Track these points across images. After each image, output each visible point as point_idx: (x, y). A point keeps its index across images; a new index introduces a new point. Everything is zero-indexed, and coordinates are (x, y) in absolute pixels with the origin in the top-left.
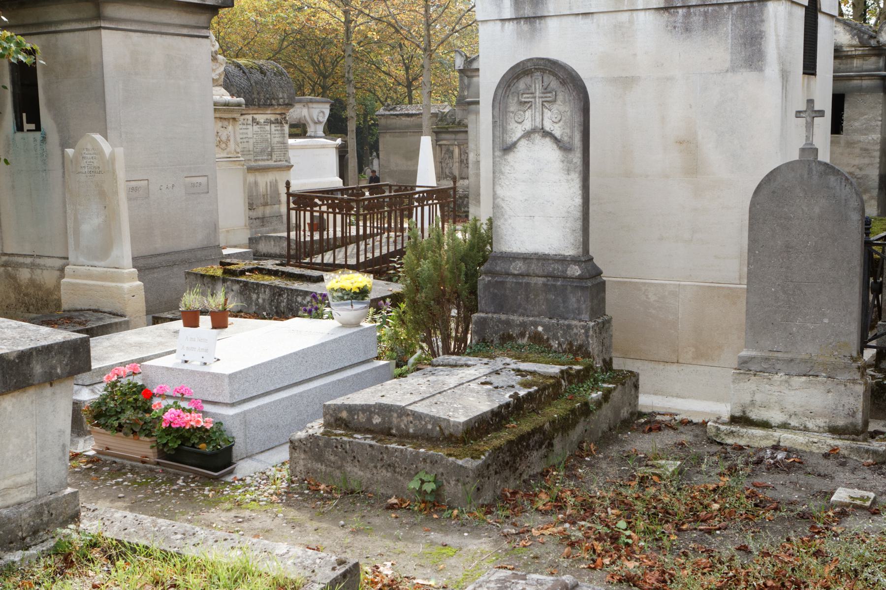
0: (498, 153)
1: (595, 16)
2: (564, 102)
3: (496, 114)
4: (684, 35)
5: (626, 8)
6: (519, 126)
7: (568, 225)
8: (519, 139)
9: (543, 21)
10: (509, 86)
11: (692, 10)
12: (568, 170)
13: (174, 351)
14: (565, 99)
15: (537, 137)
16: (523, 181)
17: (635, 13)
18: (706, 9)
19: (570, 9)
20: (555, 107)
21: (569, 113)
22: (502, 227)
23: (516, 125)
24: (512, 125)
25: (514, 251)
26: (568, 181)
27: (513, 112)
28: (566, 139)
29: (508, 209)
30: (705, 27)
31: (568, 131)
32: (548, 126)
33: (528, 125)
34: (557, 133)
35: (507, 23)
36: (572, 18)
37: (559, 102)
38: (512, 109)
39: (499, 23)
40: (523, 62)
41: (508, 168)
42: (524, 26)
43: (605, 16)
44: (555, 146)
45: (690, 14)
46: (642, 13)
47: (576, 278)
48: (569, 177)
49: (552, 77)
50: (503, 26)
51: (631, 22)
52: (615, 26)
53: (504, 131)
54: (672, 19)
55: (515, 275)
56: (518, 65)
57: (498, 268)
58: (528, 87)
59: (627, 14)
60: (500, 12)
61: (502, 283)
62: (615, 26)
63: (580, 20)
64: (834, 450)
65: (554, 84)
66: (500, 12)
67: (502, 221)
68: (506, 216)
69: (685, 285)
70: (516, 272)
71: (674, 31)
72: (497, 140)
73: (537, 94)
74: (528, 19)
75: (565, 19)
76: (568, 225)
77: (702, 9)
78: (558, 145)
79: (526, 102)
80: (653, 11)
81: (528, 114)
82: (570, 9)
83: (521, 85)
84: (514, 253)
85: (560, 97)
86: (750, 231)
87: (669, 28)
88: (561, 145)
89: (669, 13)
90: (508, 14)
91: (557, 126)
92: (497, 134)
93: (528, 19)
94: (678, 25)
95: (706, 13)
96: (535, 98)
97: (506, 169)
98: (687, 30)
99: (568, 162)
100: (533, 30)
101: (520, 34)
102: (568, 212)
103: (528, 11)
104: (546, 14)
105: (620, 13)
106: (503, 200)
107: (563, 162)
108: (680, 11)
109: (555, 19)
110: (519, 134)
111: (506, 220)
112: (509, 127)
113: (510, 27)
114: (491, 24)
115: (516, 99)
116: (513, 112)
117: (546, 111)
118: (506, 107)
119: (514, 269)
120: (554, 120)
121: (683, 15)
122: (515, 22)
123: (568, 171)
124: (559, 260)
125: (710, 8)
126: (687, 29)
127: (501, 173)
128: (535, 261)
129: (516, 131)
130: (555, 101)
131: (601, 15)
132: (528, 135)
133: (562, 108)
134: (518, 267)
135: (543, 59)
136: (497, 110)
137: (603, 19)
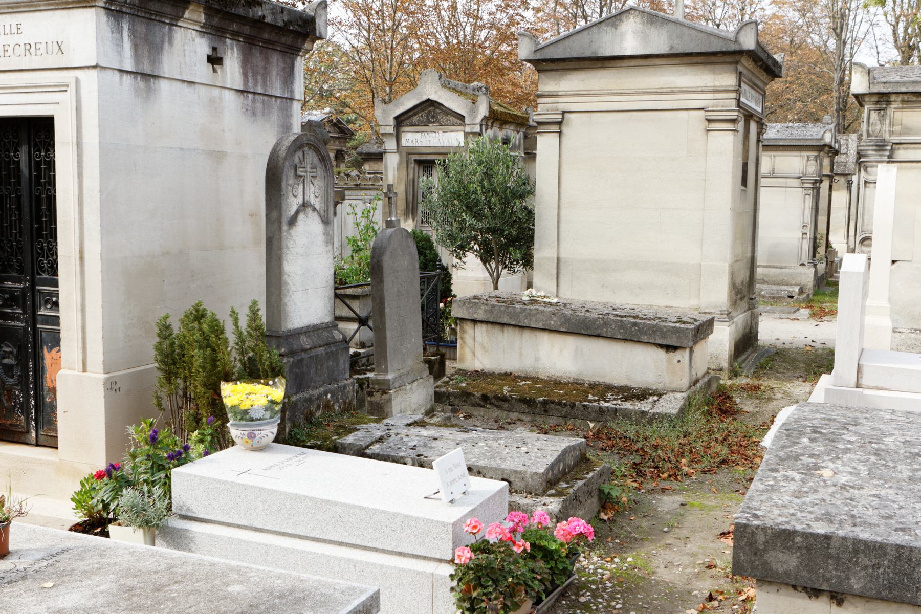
1: (197, 86)
8: (297, 213)
9: (156, 82)
11: (257, 97)
13: (84, 371)
17: (224, 91)
36: (179, 84)
39: (117, 74)
42: (141, 84)
59: (218, 90)
61: (301, 360)
63: (185, 88)
64: (621, 584)
66: (121, 62)
80: (234, 92)
84: (298, 329)
86: (297, 498)
90: (129, 66)
91: (317, 200)
103: (147, 69)
105: (213, 88)
109: (166, 81)
113: (127, 79)
114: (110, 72)
129: (292, 203)
137: (202, 90)
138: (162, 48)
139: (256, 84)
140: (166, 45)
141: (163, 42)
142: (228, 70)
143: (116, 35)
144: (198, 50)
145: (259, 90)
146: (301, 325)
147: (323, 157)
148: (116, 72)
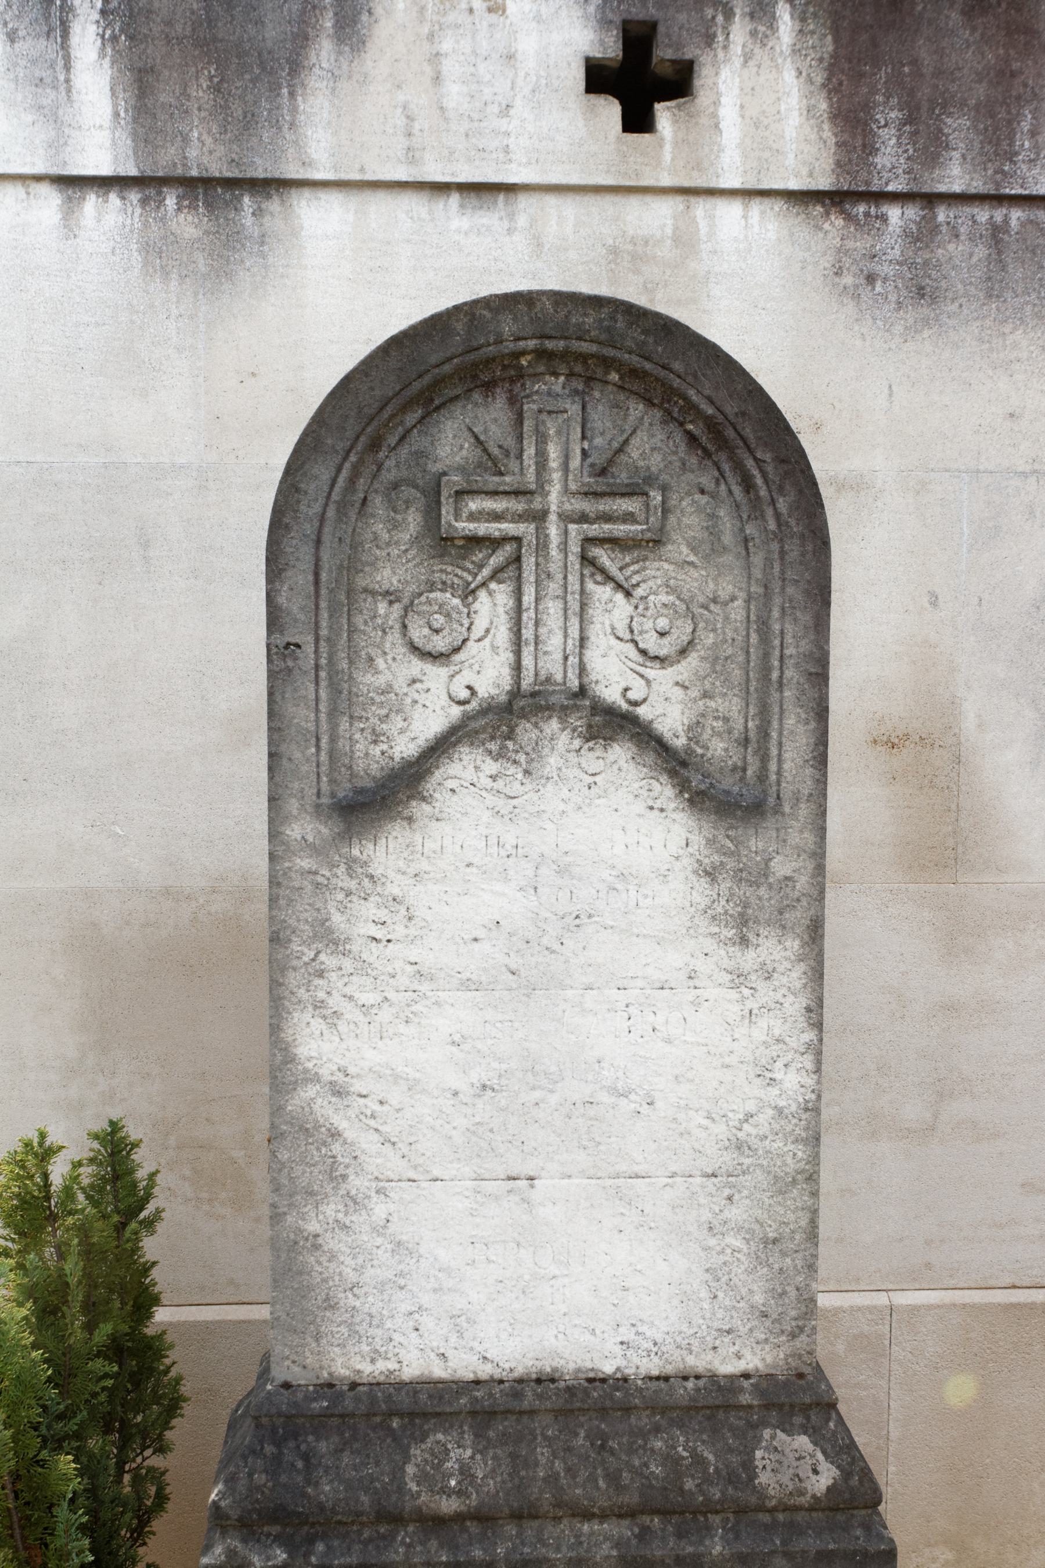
0: (302, 828)
1: (523, 201)
2: (710, 548)
3: (294, 603)
4: (910, 315)
5: (666, 181)
6: (436, 675)
7: (736, 1213)
8: (440, 748)
9: (274, 205)
10: (375, 445)
11: (942, 214)
12: (743, 921)
14: (713, 531)
15: (558, 742)
16: (468, 985)
17: (701, 207)
18: (999, 214)
19: (411, 156)
20: (654, 577)
21: (737, 611)
22: (331, 1242)
23: (416, 666)
24: (393, 669)
25: (408, 1373)
26: (739, 978)
27: (391, 596)
28: (718, 748)
29: (367, 1142)
30: (993, 287)
31: (731, 705)
32: (613, 676)
33: (487, 672)
34: (669, 712)
35: (91, 201)
36: (414, 204)
37: (679, 549)
38: (387, 577)
39: (51, 198)
40: (471, 313)
41: (370, 910)
42: (185, 223)
43: (569, 208)
44: (665, 791)
45: (935, 229)
46: (730, 211)
47: (816, 1505)
48: (749, 959)
49: (636, 409)
50: (69, 211)
51: (685, 241)
52: (614, 251)
53: (342, 700)
54: (860, 244)
55: (435, 1524)
56: (436, 326)
57: (327, 1490)
58: (490, 461)
60: (57, 145)
62: (614, 251)
65: (651, 445)
66: (57, 145)
67: (331, 1210)
68: (356, 1183)
69: (914, 1310)
70: (449, 1505)
71: (866, 293)
72: (301, 756)
73: (554, 496)
74: (199, 188)
75: (380, 204)
76: (736, 1213)
77: (983, 214)
78: (682, 786)
79: (475, 541)
81: (492, 607)
82: (411, 156)
83: (450, 443)
85: (689, 519)
87: (848, 280)
88: (696, 781)
89: (849, 218)
90: (100, 151)
91: (663, 678)
92: (301, 716)
93: (199, 188)
94: (885, 269)
95: (997, 233)
96: (540, 517)
97: (359, 920)
98: (921, 292)
99: (739, 876)
100: (227, 251)
101: (158, 254)
102: (740, 1146)
103: (203, 152)
104: (293, 172)
105: (634, 202)
106: (338, 1091)
107: (711, 874)
108: (894, 213)
109: (333, 203)
110: (431, 720)
111: (354, 1202)
112: (367, 680)
113: (106, 217)
115: (413, 520)
116: (391, 596)
117: (602, 592)
118: (352, 566)
119: (429, 1479)
120: (651, 642)
121: (906, 233)
122: (134, 196)
123: (743, 927)
124: (691, 1409)
125: (1016, 215)
126: (923, 290)
127: (327, 937)
128: (547, 1426)
130: (655, 542)
131: (551, 201)
132: (499, 722)
133: (693, 581)
134: (452, 1470)
135: (597, 302)
136: (299, 577)
138: (296, 67)
139: (930, 149)
140: (324, 51)
141: (301, 39)
142: (729, 113)
143: (32, 46)
144: (528, 45)
145: (955, 176)
146: (464, 1365)
147: (712, 426)
148: (45, 189)
